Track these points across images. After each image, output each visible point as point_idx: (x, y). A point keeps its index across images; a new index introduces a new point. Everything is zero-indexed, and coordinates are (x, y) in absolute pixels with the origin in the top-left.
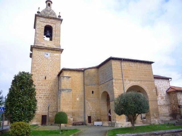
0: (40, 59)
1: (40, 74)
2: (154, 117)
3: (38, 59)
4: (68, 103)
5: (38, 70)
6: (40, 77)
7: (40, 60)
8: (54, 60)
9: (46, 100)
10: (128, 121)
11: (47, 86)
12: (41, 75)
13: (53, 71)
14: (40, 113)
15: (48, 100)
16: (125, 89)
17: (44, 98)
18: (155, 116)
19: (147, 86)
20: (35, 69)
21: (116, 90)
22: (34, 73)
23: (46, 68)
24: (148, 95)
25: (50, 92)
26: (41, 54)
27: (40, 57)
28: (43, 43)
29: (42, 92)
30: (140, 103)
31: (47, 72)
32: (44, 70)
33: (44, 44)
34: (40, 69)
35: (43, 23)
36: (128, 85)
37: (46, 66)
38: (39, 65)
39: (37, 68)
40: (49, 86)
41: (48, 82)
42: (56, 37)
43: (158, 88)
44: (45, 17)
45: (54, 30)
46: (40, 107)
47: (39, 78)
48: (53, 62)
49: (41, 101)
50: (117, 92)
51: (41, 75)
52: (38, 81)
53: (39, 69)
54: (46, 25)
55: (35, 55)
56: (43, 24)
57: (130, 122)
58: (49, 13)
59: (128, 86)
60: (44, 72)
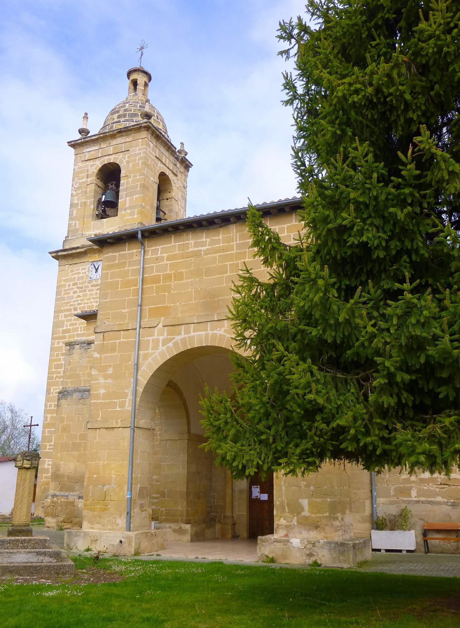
2: (295, 522)
3: (72, 294)
4: (78, 441)
7: (76, 295)
18: (306, 513)
20: (61, 329)
21: (102, 381)
26: (79, 273)
35: (91, 163)
36: (161, 348)
44: (97, 139)
50: (102, 391)
56: (92, 166)
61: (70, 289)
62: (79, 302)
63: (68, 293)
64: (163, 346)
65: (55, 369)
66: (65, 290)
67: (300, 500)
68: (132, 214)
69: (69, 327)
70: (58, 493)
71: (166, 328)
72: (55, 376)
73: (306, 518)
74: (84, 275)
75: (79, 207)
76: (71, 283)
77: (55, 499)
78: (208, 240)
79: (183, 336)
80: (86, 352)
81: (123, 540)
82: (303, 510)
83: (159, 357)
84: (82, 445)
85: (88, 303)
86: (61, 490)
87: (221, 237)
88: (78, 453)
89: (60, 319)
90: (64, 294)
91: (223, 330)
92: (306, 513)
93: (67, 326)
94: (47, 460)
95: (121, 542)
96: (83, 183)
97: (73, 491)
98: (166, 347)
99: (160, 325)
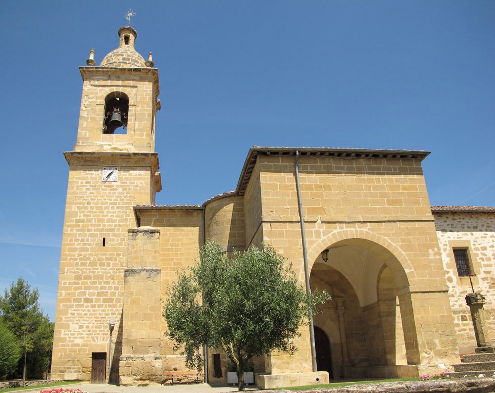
0: (87, 189)
1: (89, 230)
3: (85, 190)
5: (83, 221)
6: (87, 240)
7: (89, 192)
8: (130, 189)
9: (106, 307)
10: (319, 370)
11: (109, 265)
12: (90, 235)
13: (126, 220)
14: (86, 345)
15: (110, 306)
16: (308, 254)
17: (97, 300)
18: (438, 347)
19: (403, 240)
22: (72, 230)
23: (105, 214)
24: (407, 271)
25: (116, 282)
27: (89, 182)
28: (98, 143)
29: (92, 283)
30: (21, 287)
31: (108, 226)
32: (100, 220)
33: (102, 146)
34: (90, 216)
36: (323, 237)
37: (106, 208)
38: (86, 205)
39: (80, 216)
40: (114, 265)
41: (110, 254)
42: (136, 122)
43: (477, 249)
45: (131, 102)
46: (87, 327)
47: (84, 244)
48: (128, 193)
49: (89, 311)
51: (90, 235)
52: (82, 253)
53: (85, 218)
54: (105, 96)
55: (75, 180)
56: (100, 90)
57: (326, 373)
58: (121, 61)
59: (320, 240)
60: (99, 225)
61: (83, 186)
62: (93, 198)
63: (81, 189)
64: (324, 236)
65: (68, 251)
66: (77, 186)
67: (434, 340)
68: (141, 135)
69: (82, 218)
70: (132, 356)
71: (324, 224)
72: (69, 258)
73: (439, 351)
74: (97, 176)
75: (89, 121)
76: (84, 181)
77: (130, 361)
78: (346, 166)
79: (338, 230)
80: (149, 238)
81: (319, 378)
82: (436, 346)
83: (322, 243)
84: (154, 315)
85: (101, 200)
86: (134, 352)
87: (354, 166)
88: (150, 321)
89: (73, 210)
90: (77, 189)
91: (367, 228)
92: (438, 347)
93: (80, 216)
94: (63, 330)
95: (318, 379)
96: (93, 102)
97: (148, 353)
98: (326, 236)
99: (319, 221)
